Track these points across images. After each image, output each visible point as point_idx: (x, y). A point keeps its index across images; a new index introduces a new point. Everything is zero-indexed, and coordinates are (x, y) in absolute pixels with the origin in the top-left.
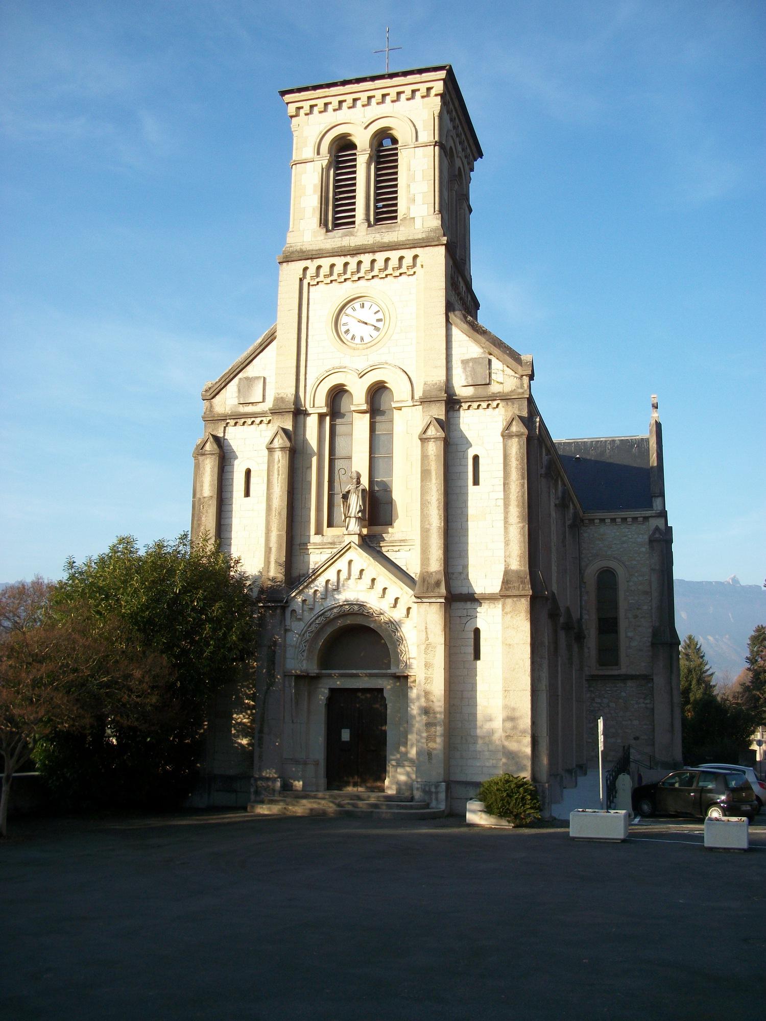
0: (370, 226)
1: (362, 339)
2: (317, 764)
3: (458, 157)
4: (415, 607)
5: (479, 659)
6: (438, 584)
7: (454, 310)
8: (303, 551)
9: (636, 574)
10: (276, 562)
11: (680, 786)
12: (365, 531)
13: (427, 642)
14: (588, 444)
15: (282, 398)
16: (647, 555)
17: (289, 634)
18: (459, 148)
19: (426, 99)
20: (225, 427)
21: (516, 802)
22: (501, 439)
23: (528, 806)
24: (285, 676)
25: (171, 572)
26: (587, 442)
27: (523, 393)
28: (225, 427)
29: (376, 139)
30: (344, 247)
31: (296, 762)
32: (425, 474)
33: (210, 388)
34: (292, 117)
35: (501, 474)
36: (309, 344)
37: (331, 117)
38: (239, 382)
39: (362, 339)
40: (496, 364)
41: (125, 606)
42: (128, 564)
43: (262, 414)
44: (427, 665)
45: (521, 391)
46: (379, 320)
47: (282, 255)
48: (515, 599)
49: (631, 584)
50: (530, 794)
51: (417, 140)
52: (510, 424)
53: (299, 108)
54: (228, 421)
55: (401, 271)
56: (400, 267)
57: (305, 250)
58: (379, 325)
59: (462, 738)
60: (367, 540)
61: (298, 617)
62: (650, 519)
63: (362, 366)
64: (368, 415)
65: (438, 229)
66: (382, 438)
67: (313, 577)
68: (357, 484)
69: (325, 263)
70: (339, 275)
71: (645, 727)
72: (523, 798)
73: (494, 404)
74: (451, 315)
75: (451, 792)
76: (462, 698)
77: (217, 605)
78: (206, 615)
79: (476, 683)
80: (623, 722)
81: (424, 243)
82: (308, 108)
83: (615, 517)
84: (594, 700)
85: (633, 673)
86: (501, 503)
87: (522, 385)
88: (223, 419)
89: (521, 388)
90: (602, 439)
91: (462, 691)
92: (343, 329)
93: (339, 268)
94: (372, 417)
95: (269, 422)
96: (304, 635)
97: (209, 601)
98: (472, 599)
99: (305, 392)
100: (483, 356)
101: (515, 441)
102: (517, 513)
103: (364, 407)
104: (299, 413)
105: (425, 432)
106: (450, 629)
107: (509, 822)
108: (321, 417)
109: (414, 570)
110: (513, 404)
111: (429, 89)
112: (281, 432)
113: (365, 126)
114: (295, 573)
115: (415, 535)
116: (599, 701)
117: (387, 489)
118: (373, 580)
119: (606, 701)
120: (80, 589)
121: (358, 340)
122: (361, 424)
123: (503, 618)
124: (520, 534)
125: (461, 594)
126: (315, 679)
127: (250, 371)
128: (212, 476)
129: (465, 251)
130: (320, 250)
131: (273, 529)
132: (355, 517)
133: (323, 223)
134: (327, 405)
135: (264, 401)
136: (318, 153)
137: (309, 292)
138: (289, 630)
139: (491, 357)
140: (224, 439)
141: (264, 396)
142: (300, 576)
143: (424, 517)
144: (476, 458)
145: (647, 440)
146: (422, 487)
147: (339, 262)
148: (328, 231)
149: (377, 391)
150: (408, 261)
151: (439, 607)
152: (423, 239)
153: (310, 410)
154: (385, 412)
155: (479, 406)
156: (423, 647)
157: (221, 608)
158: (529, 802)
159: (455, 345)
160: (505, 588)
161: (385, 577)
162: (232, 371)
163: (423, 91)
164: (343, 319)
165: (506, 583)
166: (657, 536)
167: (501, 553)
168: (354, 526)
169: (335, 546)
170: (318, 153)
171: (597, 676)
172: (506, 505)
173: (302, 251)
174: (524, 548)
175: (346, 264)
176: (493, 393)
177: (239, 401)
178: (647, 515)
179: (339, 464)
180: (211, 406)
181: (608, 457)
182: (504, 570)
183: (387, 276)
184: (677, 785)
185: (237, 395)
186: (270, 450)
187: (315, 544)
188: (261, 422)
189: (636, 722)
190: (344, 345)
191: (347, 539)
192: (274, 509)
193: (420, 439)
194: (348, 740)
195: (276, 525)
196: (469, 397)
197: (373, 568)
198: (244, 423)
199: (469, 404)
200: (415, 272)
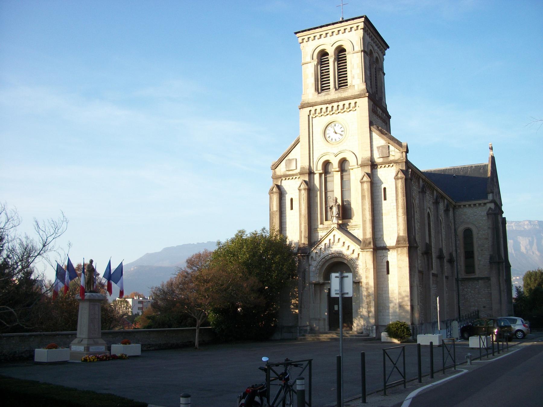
0: (336, 90)
1: (336, 140)
2: (324, 320)
3: (375, 53)
4: (361, 253)
5: (389, 274)
6: (370, 243)
7: (373, 125)
8: (316, 231)
9: (482, 230)
10: (304, 237)
11: (479, 325)
12: (340, 222)
13: (366, 268)
14: (460, 169)
15: (303, 167)
16: (486, 221)
17: (311, 267)
18: (376, 48)
19: (357, 31)
20: (281, 181)
21: (400, 332)
22: (394, 180)
23: (405, 334)
24: (310, 284)
25: (258, 244)
26: (459, 168)
27: (403, 160)
28: (281, 181)
29: (337, 50)
30: (326, 100)
31: (316, 319)
32: (363, 197)
33: (274, 164)
34: (300, 43)
35: (395, 195)
36: (314, 143)
37: (317, 42)
38: (286, 162)
39: (336, 140)
40: (392, 148)
41: (241, 259)
42: (241, 242)
43: (296, 175)
44: (367, 277)
45: (402, 159)
46: (342, 131)
47: (300, 105)
48: (402, 248)
49: (479, 235)
50: (406, 329)
51: (354, 50)
52: (398, 174)
53: (303, 39)
54: (282, 178)
55: (350, 109)
56: (349, 107)
57: (309, 102)
58: (342, 133)
59: (383, 307)
60: (341, 226)
61: (314, 259)
62: (487, 204)
63: (336, 152)
64: (339, 173)
65: (364, 90)
66: (346, 182)
67: (320, 242)
68: (336, 202)
69: (318, 108)
70: (324, 113)
71: (488, 301)
72: (403, 331)
73: (391, 165)
74: (372, 127)
75: (379, 330)
76: (382, 290)
77: (277, 257)
78: (274, 261)
79: (388, 284)
80: (478, 300)
81: (359, 96)
82: (307, 39)
83: (471, 204)
84: (464, 290)
85: (482, 277)
86: (395, 207)
87: (403, 156)
88: (280, 177)
89: (403, 158)
90: (466, 166)
91: (382, 288)
92: (327, 136)
93: (324, 110)
94: (342, 173)
95: (299, 178)
96: (317, 266)
97: (274, 255)
98: (386, 249)
99: (313, 164)
100: (386, 144)
101: (400, 181)
102: (402, 212)
103: (338, 169)
104: (311, 173)
105: (362, 179)
106: (376, 261)
107: (398, 341)
108: (320, 174)
109: (361, 238)
110: (399, 165)
111: (357, 27)
112: (304, 182)
113: (332, 45)
114: (313, 241)
115: (360, 223)
116: (466, 290)
117: (349, 204)
118: (344, 243)
119: (469, 290)
120: (223, 253)
121: (334, 140)
122: (337, 177)
123: (397, 257)
124: (403, 220)
125: (381, 247)
126: (323, 284)
127: (290, 156)
128: (277, 202)
129: (382, 94)
130: (316, 102)
131: (302, 223)
132: (335, 216)
133: (317, 90)
134: (322, 169)
135: (296, 169)
136: (313, 59)
137: (312, 121)
138: (311, 265)
139: (389, 145)
140: (281, 186)
141: (296, 166)
142: (314, 242)
143: (363, 215)
144: (385, 189)
145: (487, 165)
146: (362, 203)
147: (324, 107)
148: (319, 93)
149: (343, 162)
150: (352, 105)
151: (370, 253)
152: (358, 95)
153: (315, 172)
154: (347, 171)
155: (385, 166)
156: (365, 270)
157: (279, 257)
158: (405, 332)
159: (374, 140)
160: (398, 244)
161: (349, 241)
162: (282, 157)
163: (355, 28)
164: (327, 132)
165: (398, 241)
166: (490, 212)
167: (396, 229)
168: (335, 220)
169: (328, 229)
170: (313, 59)
171: (466, 278)
172: (397, 209)
173: (308, 103)
174: (405, 226)
175: (327, 108)
176: (391, 160)
177: (286, 169)
178: (485, 202)
179: (329, 194)
180: (275, 172)
181: (469, 174)
182: (397, 236)
183: (344, 112)
184: (478, 325)
185: (285, 167)
186: (300, 190)
187: (320, 228)
188: (296, 178)
189: (484, 299)
190: (328, 143)
191: (333, 226)
192: (302, 215)
193: (361, 182)
194: (335, 310)
195: (303, 222)
196: (381, 163)
197: (343, 237)
198: (289, 179)
199: (381, 165)
200: (356, 110)
